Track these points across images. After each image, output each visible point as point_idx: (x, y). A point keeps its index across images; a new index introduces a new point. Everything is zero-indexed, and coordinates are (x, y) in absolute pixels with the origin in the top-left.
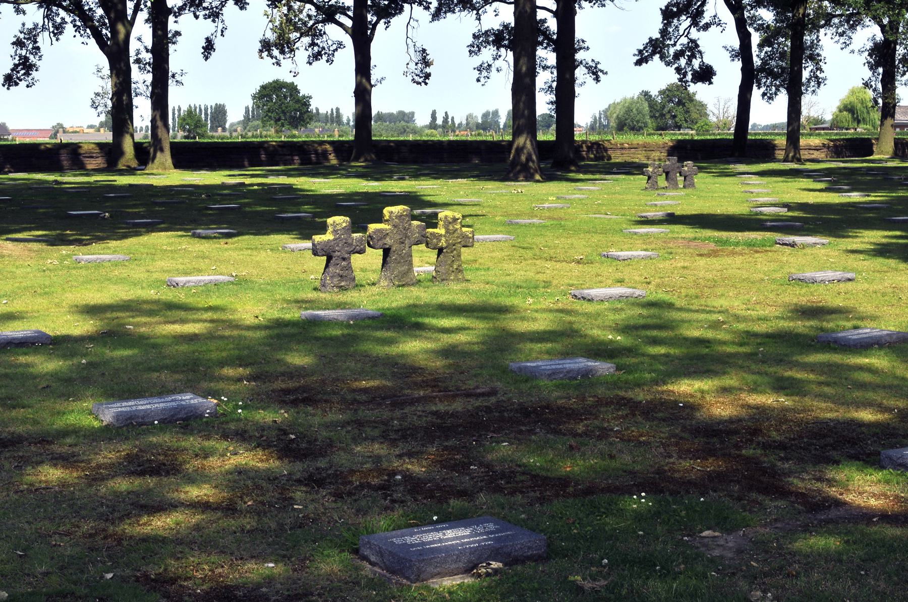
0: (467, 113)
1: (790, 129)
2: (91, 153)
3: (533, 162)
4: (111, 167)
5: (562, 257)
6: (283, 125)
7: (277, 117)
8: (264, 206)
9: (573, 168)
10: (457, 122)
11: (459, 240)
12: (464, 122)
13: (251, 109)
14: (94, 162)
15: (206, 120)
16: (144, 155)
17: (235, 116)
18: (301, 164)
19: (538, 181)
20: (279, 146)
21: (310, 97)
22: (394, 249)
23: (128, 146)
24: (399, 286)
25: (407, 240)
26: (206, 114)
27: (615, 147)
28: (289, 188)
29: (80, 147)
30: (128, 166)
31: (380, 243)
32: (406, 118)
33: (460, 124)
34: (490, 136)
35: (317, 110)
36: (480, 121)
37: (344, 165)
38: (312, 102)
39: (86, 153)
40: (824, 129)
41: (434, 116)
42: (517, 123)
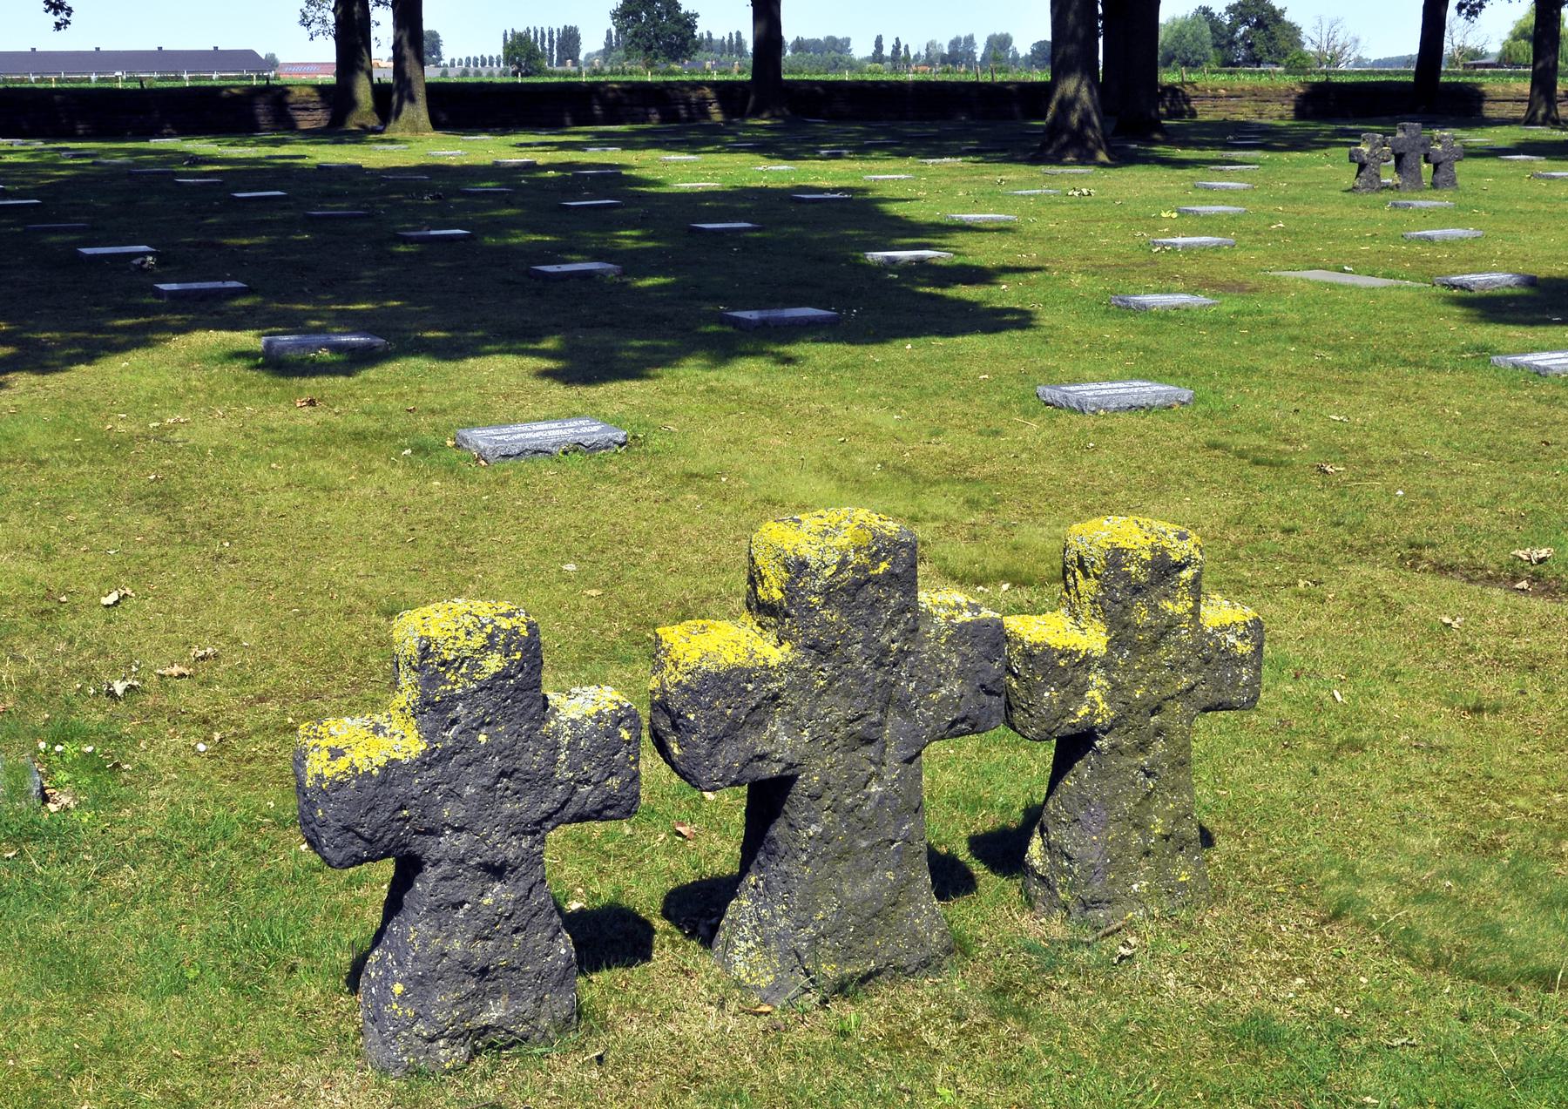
0: (928, 40)
1: (1540, 65)
2: (308, 102)
3: (1093, 127)
4: (334, 131)
5: (1457, 553)
6: (656, 57)
7: (648, 44)
8: (535, 233)
9: (1157, 136)
10: (912, 53)
11: (1185, 681)
12: (923, 53)
13: (614, 34)
14: (310, 118)
15: (551, 49)
16: (388, 101)
17: (592, 42)
18: (662, 121)
19: (1103, 165)
20: (623, 90)
21: (696, 16)
22: (810, 780)
23: (363, 92)
24: (842, 988)
25: (894, 718)
26: (551, 41)
27: (1203, 94)
28: (611, 179)
29: (288, 93)
30: (363, 126)
31: (730, 755)
32: (838, 46)
33: (917, 56)
34: (961, 75)
35: (709, 34)
36: (946, 51)
37: (734, 124)
38: (698, 21)
39: (296, 103)
40: (1487, 66)
41: (879, 43)
42: (1061, 51)
